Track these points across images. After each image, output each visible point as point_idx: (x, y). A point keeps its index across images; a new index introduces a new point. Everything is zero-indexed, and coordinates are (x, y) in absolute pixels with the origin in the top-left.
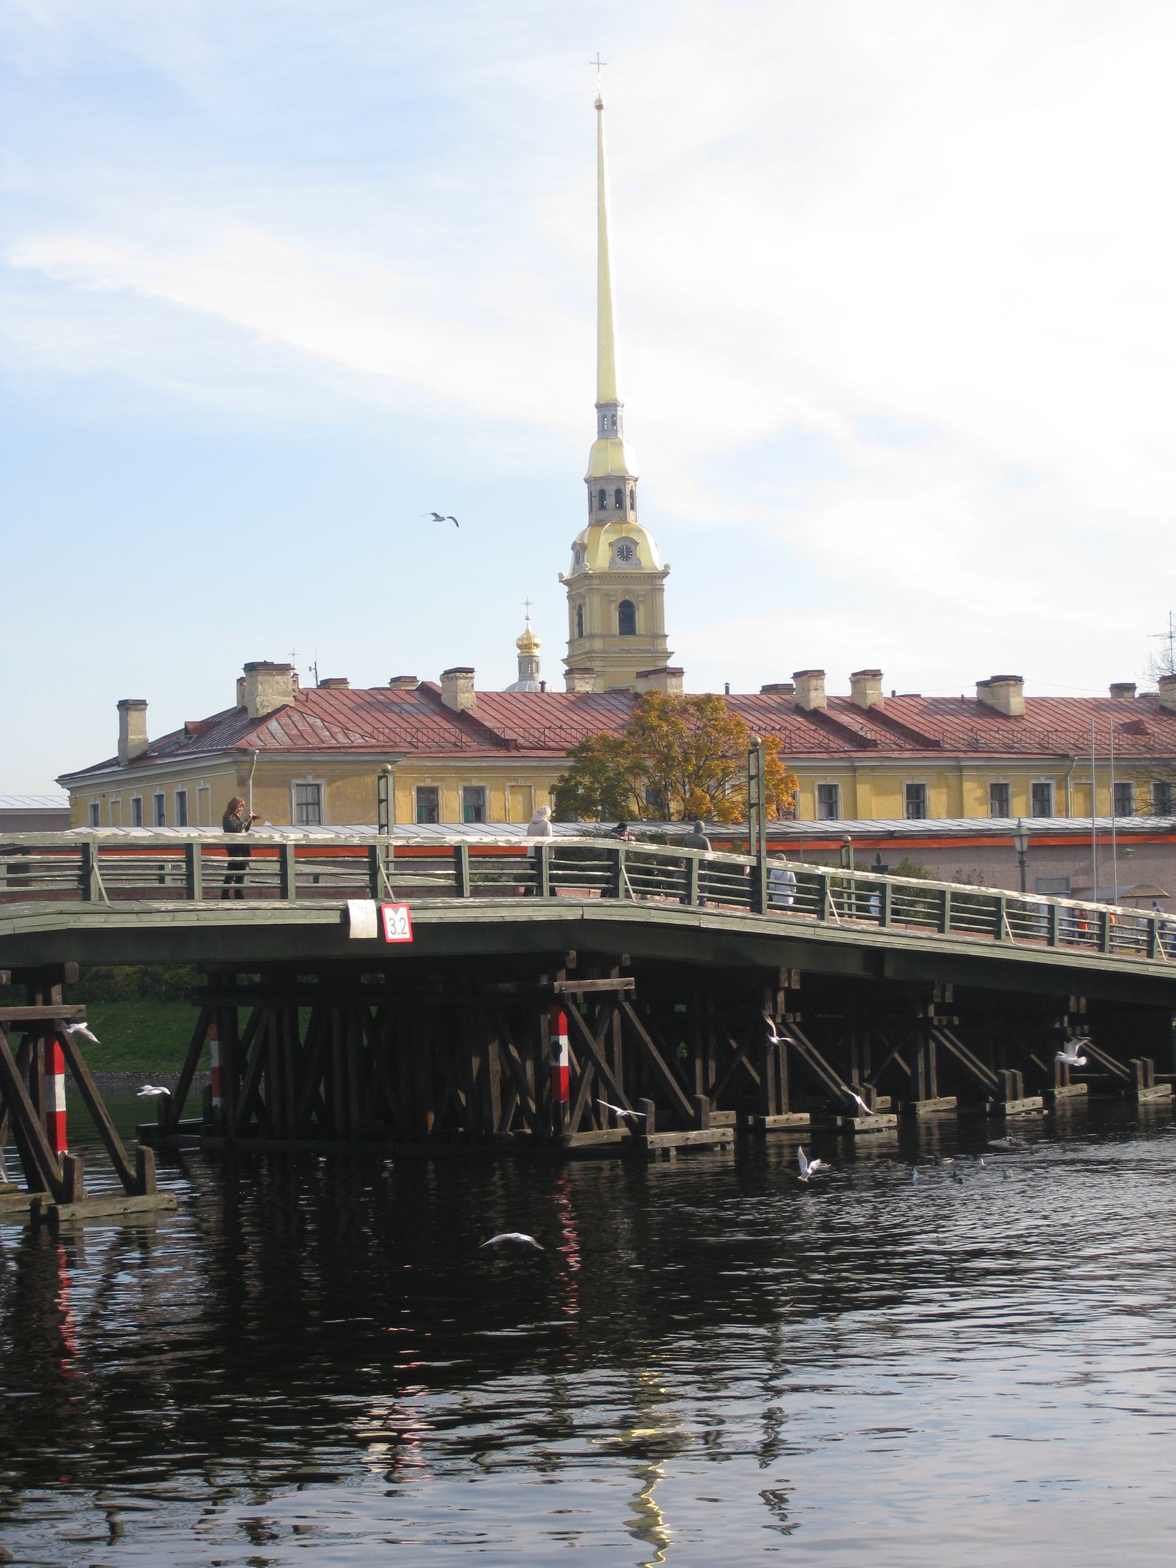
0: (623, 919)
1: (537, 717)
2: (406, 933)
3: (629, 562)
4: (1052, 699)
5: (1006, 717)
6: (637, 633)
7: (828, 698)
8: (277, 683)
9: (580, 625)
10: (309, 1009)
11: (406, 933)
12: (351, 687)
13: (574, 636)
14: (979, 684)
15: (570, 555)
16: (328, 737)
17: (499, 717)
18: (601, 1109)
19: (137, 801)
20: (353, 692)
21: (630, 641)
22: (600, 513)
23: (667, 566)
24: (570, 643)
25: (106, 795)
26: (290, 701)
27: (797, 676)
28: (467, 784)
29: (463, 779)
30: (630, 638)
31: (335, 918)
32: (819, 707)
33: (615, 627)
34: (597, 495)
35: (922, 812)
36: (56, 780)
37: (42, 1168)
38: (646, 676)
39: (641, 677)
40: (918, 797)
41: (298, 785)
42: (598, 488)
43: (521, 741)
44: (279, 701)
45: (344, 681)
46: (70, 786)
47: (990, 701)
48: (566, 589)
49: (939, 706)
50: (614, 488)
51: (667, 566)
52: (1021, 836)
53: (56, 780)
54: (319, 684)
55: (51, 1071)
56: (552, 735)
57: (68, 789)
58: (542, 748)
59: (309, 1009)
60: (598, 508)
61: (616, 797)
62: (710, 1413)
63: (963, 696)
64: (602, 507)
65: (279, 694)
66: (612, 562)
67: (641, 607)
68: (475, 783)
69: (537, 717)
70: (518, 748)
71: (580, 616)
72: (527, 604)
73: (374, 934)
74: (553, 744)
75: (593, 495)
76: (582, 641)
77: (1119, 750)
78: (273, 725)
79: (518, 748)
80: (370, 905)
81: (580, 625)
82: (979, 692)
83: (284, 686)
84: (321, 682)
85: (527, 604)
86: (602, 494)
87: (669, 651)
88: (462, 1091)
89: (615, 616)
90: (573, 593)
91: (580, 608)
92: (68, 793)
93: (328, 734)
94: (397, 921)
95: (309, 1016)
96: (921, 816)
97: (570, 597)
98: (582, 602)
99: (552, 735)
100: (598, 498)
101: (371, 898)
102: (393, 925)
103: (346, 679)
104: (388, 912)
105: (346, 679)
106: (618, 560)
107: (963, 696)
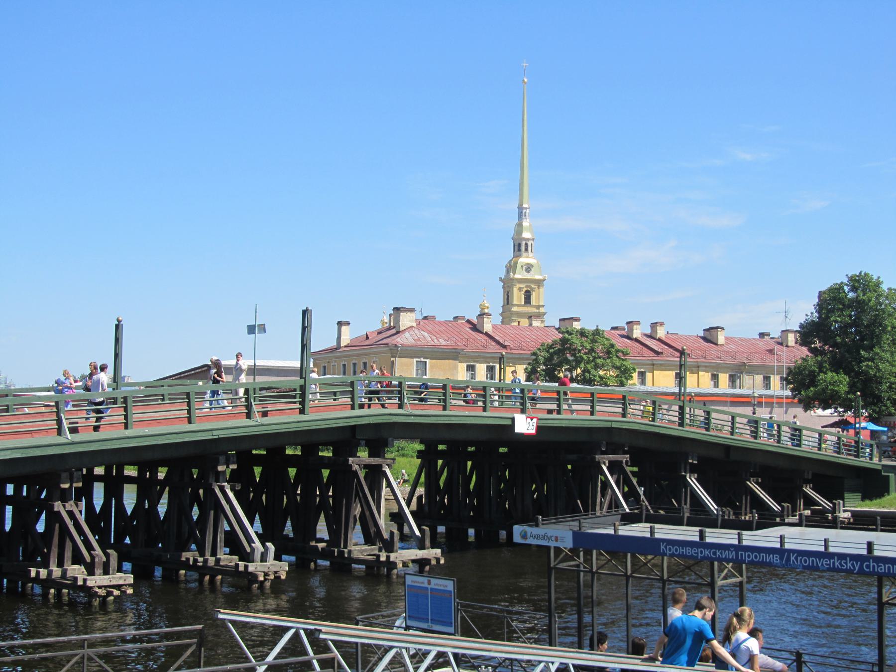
1: (517, 336)
5: (716, 344)
10: (471, 462)
14: (705, 330)
15: (504, 270)
17: (502, 335)
19: (344, 365)
20: (439, 322)
22: (518, 253)
24: (503, 307)
26: (414, 324)
27: (628, 323)
29: (486, 362)
31: (509, 422)
43: (512, 346)
44: (409, 324)
45: (434, 317)
47: (709, 338)
48: (502, 284)
49: (687, 338)
52: (754, 397)
55: (666, 512)
56: (525, 345)
59: (471, 462)
61: (853, 366)
64: (519, 250)
65: (410, 321)
67: (534, 293)
69: (517, 336)
74: (525, 348)
78: (407, 334)
82: (704, 334)
86: (519, 245)
89: (523, 296)
91: (508, 292)
95: (441, 463)
97: (503, 287)
99: (525, 345)
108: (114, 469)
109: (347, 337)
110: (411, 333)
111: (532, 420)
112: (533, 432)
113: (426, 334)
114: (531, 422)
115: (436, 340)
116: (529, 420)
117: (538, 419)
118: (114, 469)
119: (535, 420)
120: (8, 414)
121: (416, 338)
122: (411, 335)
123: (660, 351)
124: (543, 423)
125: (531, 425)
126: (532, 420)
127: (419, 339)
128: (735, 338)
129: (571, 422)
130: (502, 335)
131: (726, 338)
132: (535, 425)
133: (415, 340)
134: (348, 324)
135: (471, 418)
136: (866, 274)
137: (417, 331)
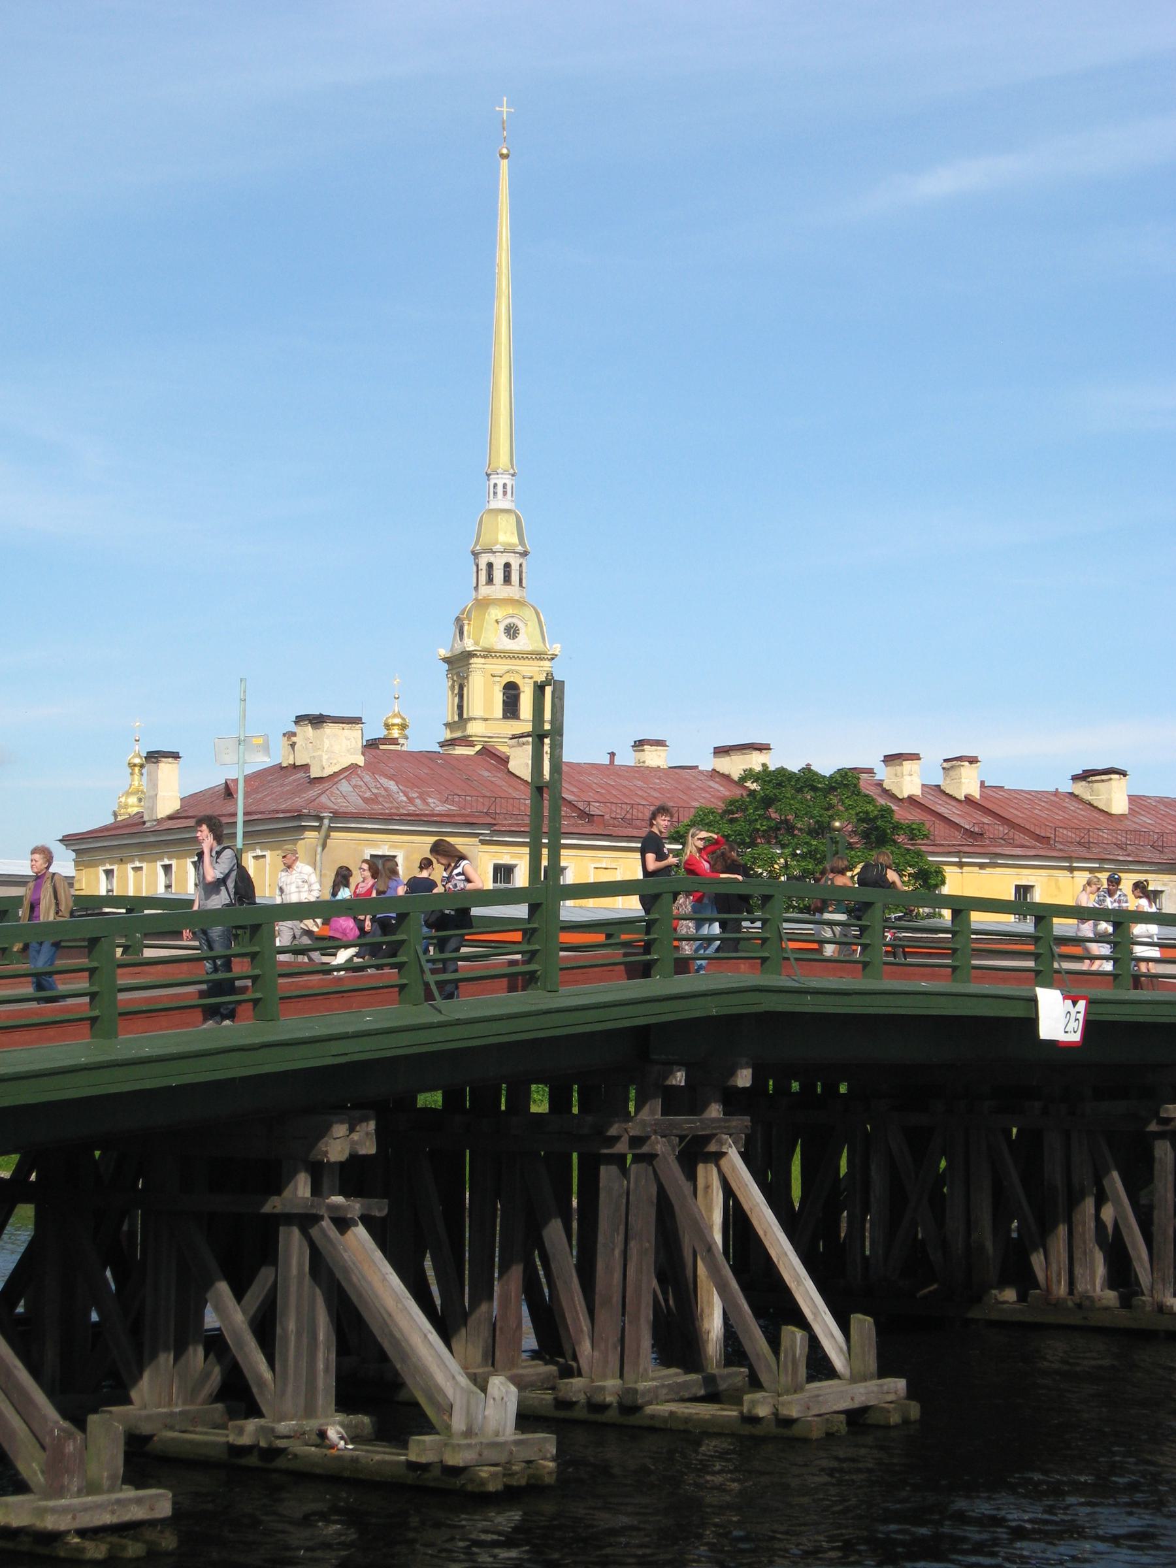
0: (138, 1086)
6: (522, 717)
16: (406, 802)
18: (252, 1312)
25: (124, 859)
32: (913, 795)
33: (498, 711)
36: (60, 840)
37: (729, 1219)
39: (719, 752)
46: (73, 848)
48: (446, 666)
50: (503, 562)
53: (60, 840)
57: (73, 850)
62: (1101, 1532)
63: (1057, 789)
78: (345, 787)
84: (367, 741)
88: (25, 1301)
89: (499, 698)
92: (73, 855)
93: (405, 799)
107: (1057, 789)
108: (575, 1094)
109: (968, 784)
110: (353, 782)
111: (1074, 1003)
112: (1076, 1037)
113: (392, 785)
114: (1073, 1011)
115: (418, 801)
116: (1069, 1002)
117: (1090, 1003)
118: (575, 1094)
119: (1082, 1004)
120: (734, 955)
121: (368, 795)
122: (355, 787)
123: (976, 829)
124: (1109, 1014)
125: (1073, 1018)
126: (1074, 1003)
127: (374, 800)
128: (1148, 797)
129: (615, 1012)
130: (575, 790)
131: (1132, 799)
132: (1081, 1017)
133: (365, 800)
134: (175, 756)
135: (942, 999)
136: (505, 629)
137: (367, 778)
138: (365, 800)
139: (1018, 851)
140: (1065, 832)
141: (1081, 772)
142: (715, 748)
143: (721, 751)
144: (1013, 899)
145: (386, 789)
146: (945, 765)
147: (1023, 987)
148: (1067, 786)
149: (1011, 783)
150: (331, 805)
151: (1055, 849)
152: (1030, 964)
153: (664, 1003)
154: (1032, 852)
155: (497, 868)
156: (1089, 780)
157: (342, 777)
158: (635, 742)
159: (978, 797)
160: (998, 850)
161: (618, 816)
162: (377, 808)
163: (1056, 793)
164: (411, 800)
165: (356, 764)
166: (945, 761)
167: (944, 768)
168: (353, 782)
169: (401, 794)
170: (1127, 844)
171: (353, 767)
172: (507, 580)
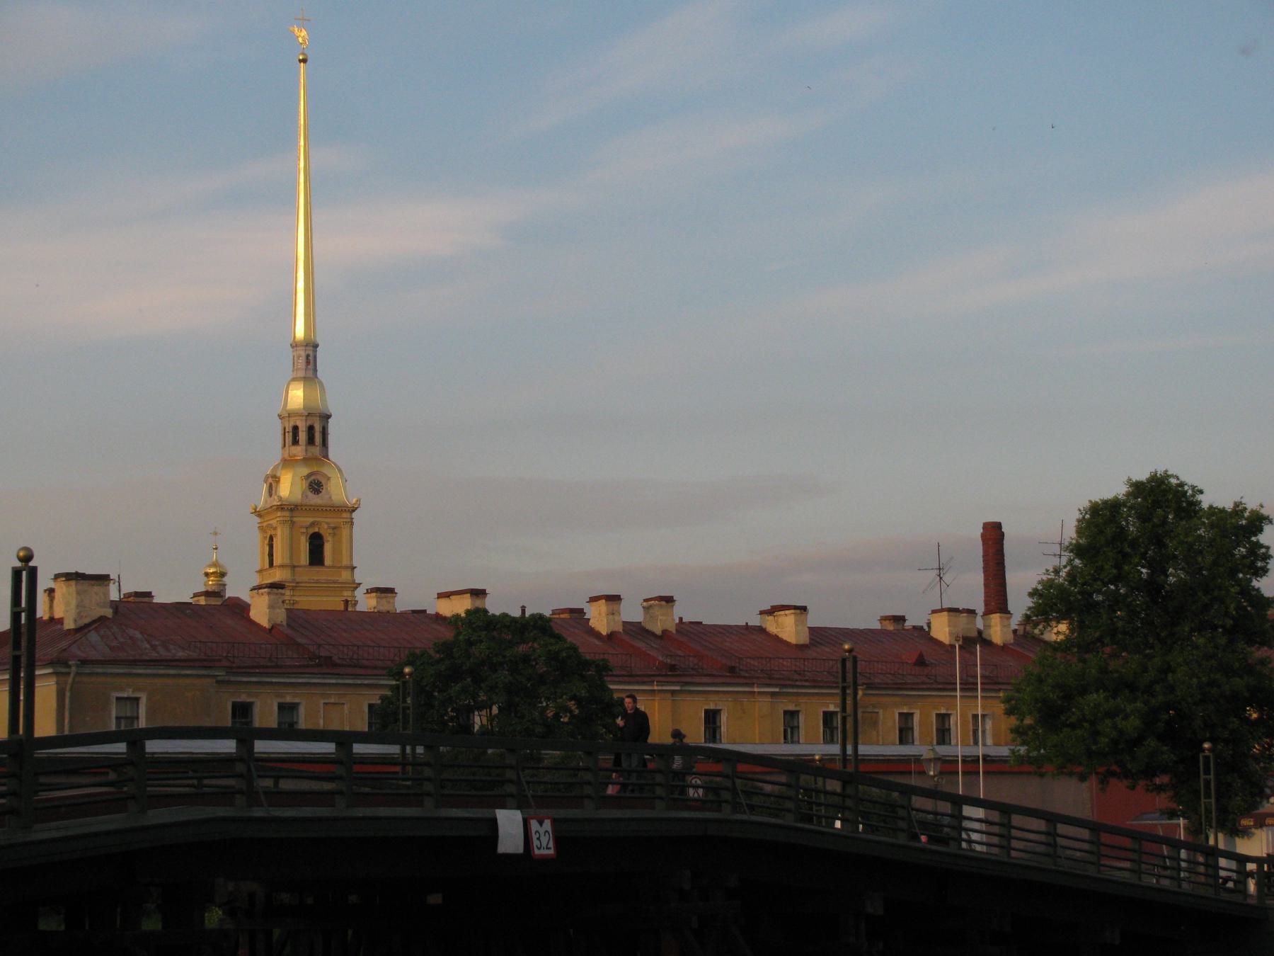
2: (550, 848)
3: (320, 495)
4: (829, 628)
7: (625, 623)
8: (96, 594)
9: (271, 555)
11: (550, 848)
12: (156, 600)
13: (264, 565)
21: (318, 573)
22: (293, 448)
23: (359, 500)
28: (281, 700)
30: (316, 569)
33: (304, 558)
34: (291, 430)
35: (718, 737)
38: (449, 597)
40: (714, 723)
41: (118, 699)
42: (292, 424)
51: (359, 500)
54: (122, 597)
58: (355, 666)
60: (291, 444)
63: (747, 623)
66: (304, 494)
68: (289, 699)
70: (335, 665)
71: (271, 547)
72: (216, 534)
73: (521, 850)
75: (287, 430)
76: (272, 571)
77: (870, 679)
79: (335, 665)
80: (517, 815)
81: (271, 555)
83: (103, 597)
84: (124, 594)
85: (216, 534)
87: (356, 582)
89: (304, 546)
90: (265, 524)
91: (271, 539)
93: (148, 646)
94: (542, 835)
96: (718, 741)
98: (273, 533)
100: (291, 434)
101: (517, 808)
102: (538, 839)
103: (150, 593)
104: (534, 825)
105: (150, 593)
106: (310, 495)
110: (102, 633)
121: (115, 644)
122: (102, 637)
133: (112, 648)
137: (115, 629)
138: (112, 648)
139: (705, 680)
140: (752, 662)
141: (769, 608)
142: (438, 594)
143: (441, 596)
144: (367, 730)
145: (131, 638)
146: (645, 604)
147: (45, 797)
148: (755, 621)
149: (710, 618)
150: (79, 653)
151: (739, 677)
152: (42, 779)
153: (1069, 841)
154: (721, 680)
155: (236, 706)
156: (775, 614)
157: (91, 628)
158: (367, 590)
159: (674, 632)
160: (689, 679)
161: (346, 657)
162: (122, 655)
163: (747, 627)
164: (154, 647)
165: (105, 617)
166: (646, 600)
167: (644, 607)
168: (102, 633)
169: (145, 642)
170: (804, 671)
171: (102, 619)
172: (311, 440)
